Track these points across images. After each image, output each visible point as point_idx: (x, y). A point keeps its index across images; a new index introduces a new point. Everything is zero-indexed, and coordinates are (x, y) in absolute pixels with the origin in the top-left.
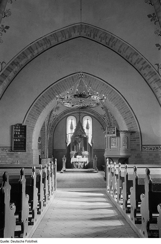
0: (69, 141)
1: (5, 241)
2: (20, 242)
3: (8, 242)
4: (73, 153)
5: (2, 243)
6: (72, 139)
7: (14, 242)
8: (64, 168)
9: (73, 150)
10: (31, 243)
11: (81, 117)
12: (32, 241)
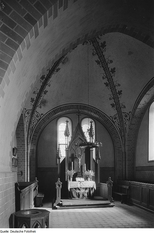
0: (63, 154)
1: (5, 232)
2: (19, 232)
3: (7, 232)
6: (67, 151)
7: (13, 232)
8: (59, 200)
9: (70, 169)
12: (31, 231)
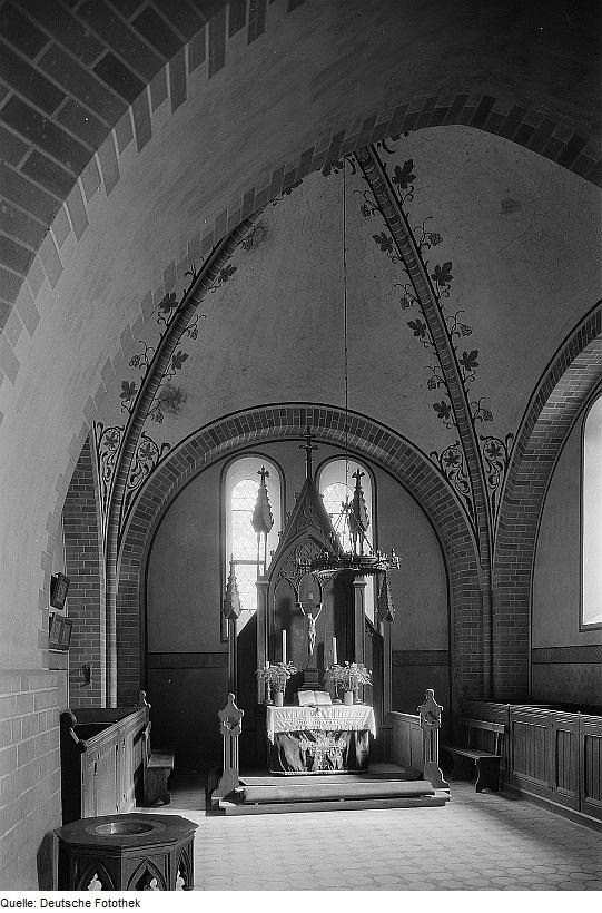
0: (248, 601)
1: (18, 904)
2: (75, 904)
3: (29, 904)
4: (273, 673)
5: (9, 910)
6: (265, 588)
7: (51, 904)
8: (231, 777)
10: (118, 909)
11: (317, 456)
12: (121, 903)
